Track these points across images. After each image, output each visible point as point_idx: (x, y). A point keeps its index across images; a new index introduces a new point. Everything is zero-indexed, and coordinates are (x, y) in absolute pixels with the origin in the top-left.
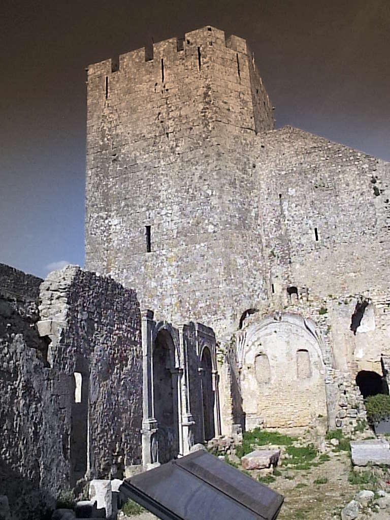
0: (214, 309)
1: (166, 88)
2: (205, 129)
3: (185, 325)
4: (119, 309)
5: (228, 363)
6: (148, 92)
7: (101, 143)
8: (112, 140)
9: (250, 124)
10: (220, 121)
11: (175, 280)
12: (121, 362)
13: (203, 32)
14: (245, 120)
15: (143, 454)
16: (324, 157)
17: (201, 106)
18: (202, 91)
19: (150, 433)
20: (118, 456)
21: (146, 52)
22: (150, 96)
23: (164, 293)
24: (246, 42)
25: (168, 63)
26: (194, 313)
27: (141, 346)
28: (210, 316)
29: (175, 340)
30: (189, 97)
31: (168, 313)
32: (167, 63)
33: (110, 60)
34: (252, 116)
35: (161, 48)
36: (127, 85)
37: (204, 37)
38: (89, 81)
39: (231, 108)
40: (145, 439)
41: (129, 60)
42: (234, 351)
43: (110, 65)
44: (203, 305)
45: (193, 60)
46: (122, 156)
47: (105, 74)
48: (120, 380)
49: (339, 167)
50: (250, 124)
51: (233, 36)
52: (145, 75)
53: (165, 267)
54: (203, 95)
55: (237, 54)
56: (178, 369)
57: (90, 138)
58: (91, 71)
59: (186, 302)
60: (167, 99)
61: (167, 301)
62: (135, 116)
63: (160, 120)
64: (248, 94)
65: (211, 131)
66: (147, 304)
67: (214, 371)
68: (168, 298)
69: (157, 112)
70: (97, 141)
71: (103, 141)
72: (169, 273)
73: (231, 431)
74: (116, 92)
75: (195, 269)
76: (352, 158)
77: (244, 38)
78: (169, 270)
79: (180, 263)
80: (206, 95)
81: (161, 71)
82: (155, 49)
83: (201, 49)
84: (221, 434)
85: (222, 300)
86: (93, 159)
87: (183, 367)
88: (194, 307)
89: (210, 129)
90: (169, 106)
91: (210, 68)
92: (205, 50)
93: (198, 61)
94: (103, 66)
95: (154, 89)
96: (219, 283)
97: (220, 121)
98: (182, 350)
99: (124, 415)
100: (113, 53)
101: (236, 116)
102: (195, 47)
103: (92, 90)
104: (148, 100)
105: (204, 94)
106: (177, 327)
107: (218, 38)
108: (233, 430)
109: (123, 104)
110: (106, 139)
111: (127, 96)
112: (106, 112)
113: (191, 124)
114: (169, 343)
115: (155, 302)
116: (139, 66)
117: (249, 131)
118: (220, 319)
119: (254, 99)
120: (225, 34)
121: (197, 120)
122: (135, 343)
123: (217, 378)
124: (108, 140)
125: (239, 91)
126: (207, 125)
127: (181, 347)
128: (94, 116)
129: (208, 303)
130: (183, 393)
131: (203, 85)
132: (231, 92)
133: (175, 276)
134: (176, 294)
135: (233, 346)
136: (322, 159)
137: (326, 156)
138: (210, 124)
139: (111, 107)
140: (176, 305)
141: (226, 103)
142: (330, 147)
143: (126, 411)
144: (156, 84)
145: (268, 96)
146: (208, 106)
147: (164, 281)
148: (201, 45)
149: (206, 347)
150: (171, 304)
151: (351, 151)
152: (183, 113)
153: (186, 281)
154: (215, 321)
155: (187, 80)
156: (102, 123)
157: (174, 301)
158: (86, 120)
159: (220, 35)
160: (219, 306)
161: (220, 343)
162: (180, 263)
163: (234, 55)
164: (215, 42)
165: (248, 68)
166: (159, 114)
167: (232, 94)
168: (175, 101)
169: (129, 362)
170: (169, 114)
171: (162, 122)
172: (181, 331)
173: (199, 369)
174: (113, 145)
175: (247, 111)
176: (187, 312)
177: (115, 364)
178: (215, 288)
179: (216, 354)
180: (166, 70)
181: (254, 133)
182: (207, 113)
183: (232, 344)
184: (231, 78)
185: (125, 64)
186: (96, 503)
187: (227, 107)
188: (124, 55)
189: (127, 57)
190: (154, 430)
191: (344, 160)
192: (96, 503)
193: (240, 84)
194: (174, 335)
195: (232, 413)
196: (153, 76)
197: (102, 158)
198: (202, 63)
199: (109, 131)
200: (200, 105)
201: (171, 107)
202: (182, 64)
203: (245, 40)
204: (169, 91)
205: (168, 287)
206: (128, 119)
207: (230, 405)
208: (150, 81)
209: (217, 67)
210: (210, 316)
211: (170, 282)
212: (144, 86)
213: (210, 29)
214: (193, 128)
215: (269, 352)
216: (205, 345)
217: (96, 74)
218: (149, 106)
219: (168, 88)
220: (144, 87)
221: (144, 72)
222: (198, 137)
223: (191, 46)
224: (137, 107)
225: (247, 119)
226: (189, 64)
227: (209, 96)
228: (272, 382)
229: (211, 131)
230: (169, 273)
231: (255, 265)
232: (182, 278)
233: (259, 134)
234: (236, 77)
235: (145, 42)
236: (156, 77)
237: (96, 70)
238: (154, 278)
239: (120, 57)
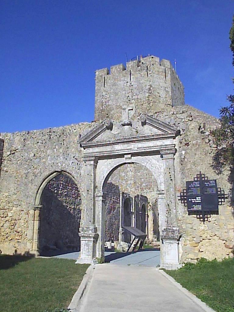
0: (149, 187)
1: (132, 85)
2: (149, 106)
3: (135, 196)
4: (114, 192)
5: (153, 211)
6: (124, 86)
7: (101, 108)
8: (106, 107)
9: (169, 103)
10: (156, 102)
11: (133, 173)
12: (114, 209)
13: (149, 59)
14: (167, 100)
15: (119, 239)
16: (202, 120)
17: (147, 95)
18: (148, 87)
19: (122, 232)
20: (112, 238)
21: (123, 66)
22: (124, 87)
23: (128, 178)
24: (170, 62)
25: (133, 72)
26: (141, 188)
27: (120, 204)
28: (147, 190)
29: (131, 202)
30: (142, 89)
31: (129, 188)
32: (132, 72)
33: (106, 68)
34: (171, 98)
35: (130, 65)
36: (114, 81)
37: (150, 61)
38: (96, 78)
39: (161, 96)
40: (120, 234)
41: (116, 69)
42: (156, 205)
43: (106, 71)
44: (145, 185)
45: (144, 72)
46: (111, 115)
47: (104, 75)
48: (113, 215)
49: (208, 125)
50: (169, 103)
51: (163, 59)
52: (122, 77)
53: (128, 167)
54: (148, 90)
55: (165, 69)
56: (132, 212)
57: (96, 105)
58: (97, 73)
59: (137, 183)
60: (132, 90)
61: (129, 182)
62: (117, 97)
63: (129, 99)
64: (169, 88)
65: (151, 107)
66: (120, 183)
67: (146, 213)
68: (129, 181)
69: (128, 96)
70: (99, 107)
71: (102, 107)
72: (131, 170)
73: (152, 237)
74: (109, 84)
75: (142, 169)
76: (214, 122)
77: (169, 60)
78: (130, 169)
79: (135, 166)
80: (150, 89)
81: (130, 76)
82: (127, 65)
83: (148, 67)
84: (148, 238)
85: (153, 183)
86: (97, 115)
87: (134, 211)
88: (141, 185)
89: (151, 105)
90: (133, 93)
91: (152, 76)
92: (150, 67)
93: (146, 72)
94: (103, 71)
95: (126, 85)
97: (156, 102)
98: (133, 205)
99: (114, 226)
100: (108, 65)
101: (163, 99)
102: (145, 66)
103: (97, 83)
104: (123, 89)
105: (149, 89)
106: (132, 197)
107: (156, 61)
108: (153, 237)
109: (112, 91)
110: (103, 107)
111: (114, 87)
112: (104, 94)
113: (142, 102)
114: (129, 203)
115: (124, 183)
116: (119, 72)
117: (169, 106)
118: (152, 191)
119: (172, 88)
120: (160, 59)
121: (145, 101)
122: (118, 203)
123: (148, 216)
124: (104, 107)
125: (165, 86)
126: (149, 104)
127: (133, 204)
128: (99, 95)
129: (147, 184)
130: (134, 221)
131: (148, 84)
132: (161, 88)
133: (133, 171)
134: (133, 180)
135: (156, 204)
136: (201, 121)
137: (203, 120)
138: (151, 103)
139: (106, 91)
140: (133, 184)
141: (158, 93)
142: (205, 116)
143: (114, 224)
144: (127, 82)
145: (181, 83)
146: (150, 95)
147: (128, 174)
148: (148, 65)
149: (144, 204)
150: (131, 184)
151: (214, 118)
152: (139, 97)
153: (137, 174)
154: (149, 192)
155: (141, 82)
156: (102, 99)
157: (132, 182)
158: (95, 97)
159: (157, 59)
160: (151, 186)
161: (150, 202)
162: (135, 166)
163: (163, 69)
164: (155, 64)
165: (170, 75)
166: (128, 96)
167: (162, 89)
168: (135, 91)
169: (116, 209)
170: (132, 97)
171: (129, 100)
172: (134, 198)
173: (140, 212)
174: (107, 109)
175: (168, 96)
176: (137, 187)
177: (112, 210)
178: (150, 178)
179: (148, 207)
180: (132, 76)
181: (171, 106)
182: (150, 98)
183: (155, 203)
184: (161, 81)
185: (113, 71)
186: (108, 247)
187: (159, 95)
188: (113, 67)
189: (114, 68)
190: (123, 232)
191: (211, 122)
192: (108, 247)
193: (166, 83)
194: (131, 199)
195: (153, 230)
196: (126, 78)
197: (102, 116)
198: (148, 74)
199: (105, 103)
200: (147, 94)
201: (133, 94)
202: (140, 74)
203: (169, 61)
204: (133, 86)
205: (130, 176)
206: (114, 98)
207: (152, 227)
208: (124, 80)
209: (155, 76)
210: (147, 190)
211: (131, 174)
212: (122, 83)
213: (153, 58)
214: (144, 104)
216: (143, 203)
217: (100, 75)
218: (124, 92)
219: (133, 85)
220: (122, 83)
221: (122, 76)
222: (145, 109)
223: (144, 65)
224: (118, 92)
225: (168, 100)
226: (142, 73)
227: (151, 90)
229: (151, 107)
230: (131, 170)
232: (136, 172)
233: (173, 107)
234: (164, 80)
235: (123, 60)
236: (127, 79)
237: (100, 73)
238: (124, 172)
239: (111, 68)
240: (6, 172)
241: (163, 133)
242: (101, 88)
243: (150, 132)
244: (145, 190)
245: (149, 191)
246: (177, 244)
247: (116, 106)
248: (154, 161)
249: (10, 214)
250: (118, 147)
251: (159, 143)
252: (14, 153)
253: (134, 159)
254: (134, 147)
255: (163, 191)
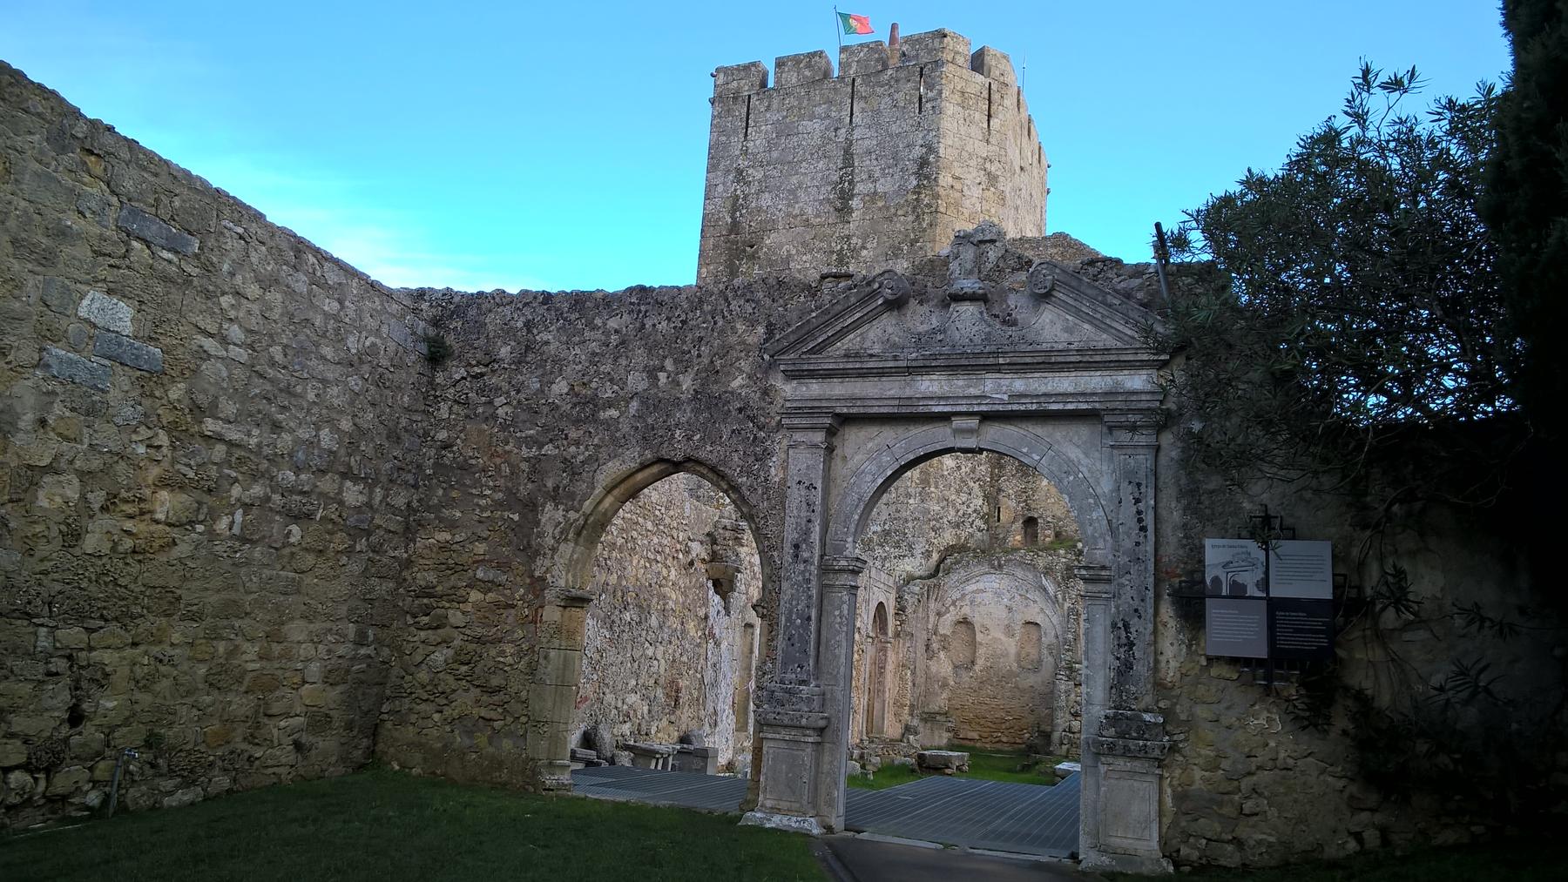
18: (918, 152)
65: (924, 230)
96: (909, 496)
131: (920, 142)
212: (816, 126)
215: (977, 620)
228: (977, 668)
229: (924, 230)
231: (973, 470)
240: (444, 448)
241: (1119, 345)
242: (734, 139)
243: (1065, 337)
244: (879, 551)
245: (896, 552)
246: (1155, 780)
247: (789, 215)
248: (1074, 453)
249: (456, 617)
250: (929, 384)
251: (1096, 381)
252: (482, 375)
253: (994, 434)
254: (998, 388)
255: (1104, 568)
